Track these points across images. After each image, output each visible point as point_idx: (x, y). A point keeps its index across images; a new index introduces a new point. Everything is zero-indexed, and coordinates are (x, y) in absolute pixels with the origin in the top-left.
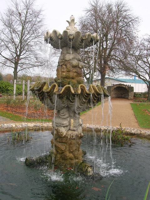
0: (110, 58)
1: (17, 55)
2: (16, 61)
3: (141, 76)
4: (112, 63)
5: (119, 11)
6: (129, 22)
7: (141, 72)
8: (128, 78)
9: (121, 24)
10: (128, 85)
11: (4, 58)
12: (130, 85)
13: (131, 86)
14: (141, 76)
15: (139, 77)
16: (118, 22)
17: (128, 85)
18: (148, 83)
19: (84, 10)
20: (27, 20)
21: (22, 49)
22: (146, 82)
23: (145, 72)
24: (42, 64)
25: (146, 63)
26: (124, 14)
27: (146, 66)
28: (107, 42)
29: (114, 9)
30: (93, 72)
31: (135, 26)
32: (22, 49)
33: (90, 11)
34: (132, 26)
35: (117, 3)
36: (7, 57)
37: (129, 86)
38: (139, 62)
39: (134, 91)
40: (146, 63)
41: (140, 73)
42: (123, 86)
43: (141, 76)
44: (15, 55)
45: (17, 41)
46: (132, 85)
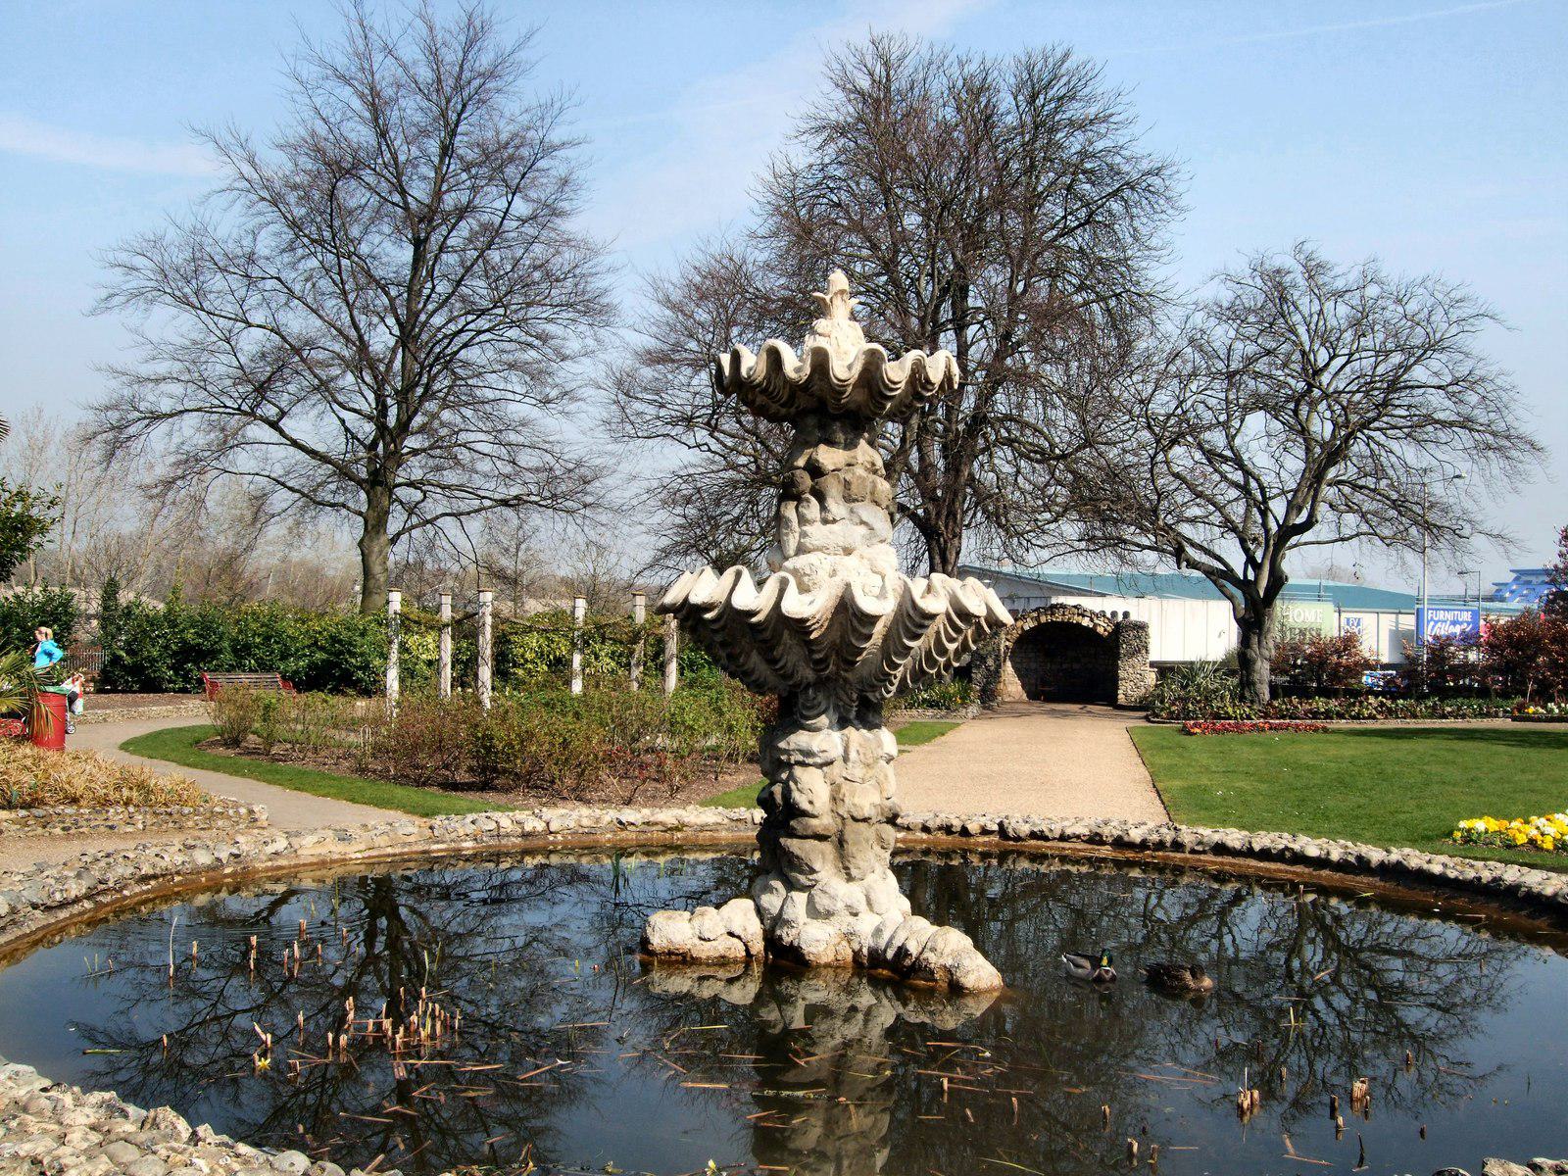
0: (986, 440)
1: (382, 428)
2: (372, 477)
3: (1189, 550)
4: (996, 467)
5: (1042, 126)
6: (1114, 191)
7: (1193, 521)
8: (1104, 564)
9: (1054, 209)
10: (1114, 614)
11: (301, 456)
12: (1126, 615)
13: (1133, 617)
14: (1193, 545)
15: (1179, 553)
16: (1033, 201)
17: (1114, 614)
18: (1238, 594)
19: (804, 126)
20: (450, 201)
21: (420, 391)
22: (1229, 585)
23: (1216, 518)
24: (563, 490)
25: (1226, 459)
26: (1075, 144)
27: (1224, 478)
28: (960, 328)
29: (1008, 109)
30: (107, 905)
31: (1142, 224)
32: (420, 391)
33: (841, 130)
34: (1122, 228)
35: (1025, 76)
36: (321, 448)
37: (1120, 618)
38: (1181, 456)
39: (1151, 647)
40: (1226, 459)
41: (1186, 529)
42: (1076, 619)
43: (1193, 545)
44: (368, 429)
45: (382, 339)
46: (1139, 609)
